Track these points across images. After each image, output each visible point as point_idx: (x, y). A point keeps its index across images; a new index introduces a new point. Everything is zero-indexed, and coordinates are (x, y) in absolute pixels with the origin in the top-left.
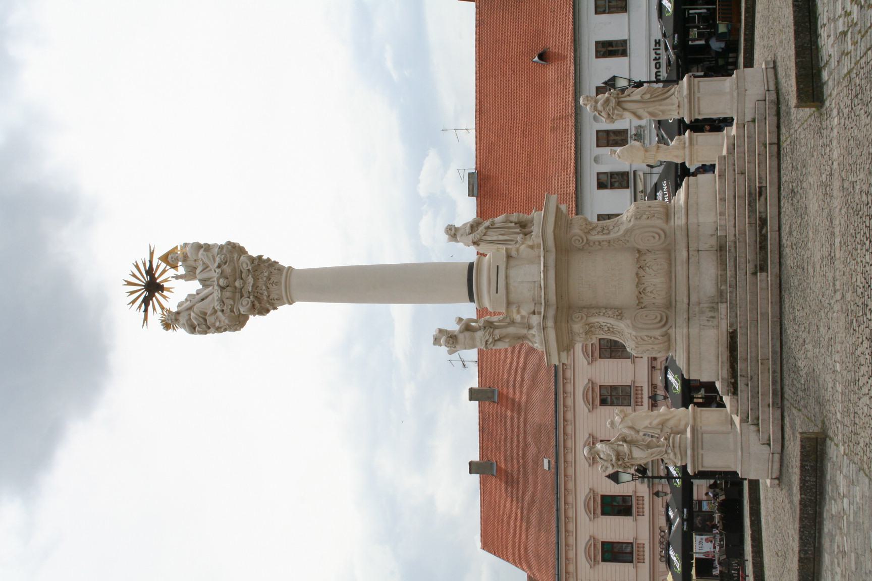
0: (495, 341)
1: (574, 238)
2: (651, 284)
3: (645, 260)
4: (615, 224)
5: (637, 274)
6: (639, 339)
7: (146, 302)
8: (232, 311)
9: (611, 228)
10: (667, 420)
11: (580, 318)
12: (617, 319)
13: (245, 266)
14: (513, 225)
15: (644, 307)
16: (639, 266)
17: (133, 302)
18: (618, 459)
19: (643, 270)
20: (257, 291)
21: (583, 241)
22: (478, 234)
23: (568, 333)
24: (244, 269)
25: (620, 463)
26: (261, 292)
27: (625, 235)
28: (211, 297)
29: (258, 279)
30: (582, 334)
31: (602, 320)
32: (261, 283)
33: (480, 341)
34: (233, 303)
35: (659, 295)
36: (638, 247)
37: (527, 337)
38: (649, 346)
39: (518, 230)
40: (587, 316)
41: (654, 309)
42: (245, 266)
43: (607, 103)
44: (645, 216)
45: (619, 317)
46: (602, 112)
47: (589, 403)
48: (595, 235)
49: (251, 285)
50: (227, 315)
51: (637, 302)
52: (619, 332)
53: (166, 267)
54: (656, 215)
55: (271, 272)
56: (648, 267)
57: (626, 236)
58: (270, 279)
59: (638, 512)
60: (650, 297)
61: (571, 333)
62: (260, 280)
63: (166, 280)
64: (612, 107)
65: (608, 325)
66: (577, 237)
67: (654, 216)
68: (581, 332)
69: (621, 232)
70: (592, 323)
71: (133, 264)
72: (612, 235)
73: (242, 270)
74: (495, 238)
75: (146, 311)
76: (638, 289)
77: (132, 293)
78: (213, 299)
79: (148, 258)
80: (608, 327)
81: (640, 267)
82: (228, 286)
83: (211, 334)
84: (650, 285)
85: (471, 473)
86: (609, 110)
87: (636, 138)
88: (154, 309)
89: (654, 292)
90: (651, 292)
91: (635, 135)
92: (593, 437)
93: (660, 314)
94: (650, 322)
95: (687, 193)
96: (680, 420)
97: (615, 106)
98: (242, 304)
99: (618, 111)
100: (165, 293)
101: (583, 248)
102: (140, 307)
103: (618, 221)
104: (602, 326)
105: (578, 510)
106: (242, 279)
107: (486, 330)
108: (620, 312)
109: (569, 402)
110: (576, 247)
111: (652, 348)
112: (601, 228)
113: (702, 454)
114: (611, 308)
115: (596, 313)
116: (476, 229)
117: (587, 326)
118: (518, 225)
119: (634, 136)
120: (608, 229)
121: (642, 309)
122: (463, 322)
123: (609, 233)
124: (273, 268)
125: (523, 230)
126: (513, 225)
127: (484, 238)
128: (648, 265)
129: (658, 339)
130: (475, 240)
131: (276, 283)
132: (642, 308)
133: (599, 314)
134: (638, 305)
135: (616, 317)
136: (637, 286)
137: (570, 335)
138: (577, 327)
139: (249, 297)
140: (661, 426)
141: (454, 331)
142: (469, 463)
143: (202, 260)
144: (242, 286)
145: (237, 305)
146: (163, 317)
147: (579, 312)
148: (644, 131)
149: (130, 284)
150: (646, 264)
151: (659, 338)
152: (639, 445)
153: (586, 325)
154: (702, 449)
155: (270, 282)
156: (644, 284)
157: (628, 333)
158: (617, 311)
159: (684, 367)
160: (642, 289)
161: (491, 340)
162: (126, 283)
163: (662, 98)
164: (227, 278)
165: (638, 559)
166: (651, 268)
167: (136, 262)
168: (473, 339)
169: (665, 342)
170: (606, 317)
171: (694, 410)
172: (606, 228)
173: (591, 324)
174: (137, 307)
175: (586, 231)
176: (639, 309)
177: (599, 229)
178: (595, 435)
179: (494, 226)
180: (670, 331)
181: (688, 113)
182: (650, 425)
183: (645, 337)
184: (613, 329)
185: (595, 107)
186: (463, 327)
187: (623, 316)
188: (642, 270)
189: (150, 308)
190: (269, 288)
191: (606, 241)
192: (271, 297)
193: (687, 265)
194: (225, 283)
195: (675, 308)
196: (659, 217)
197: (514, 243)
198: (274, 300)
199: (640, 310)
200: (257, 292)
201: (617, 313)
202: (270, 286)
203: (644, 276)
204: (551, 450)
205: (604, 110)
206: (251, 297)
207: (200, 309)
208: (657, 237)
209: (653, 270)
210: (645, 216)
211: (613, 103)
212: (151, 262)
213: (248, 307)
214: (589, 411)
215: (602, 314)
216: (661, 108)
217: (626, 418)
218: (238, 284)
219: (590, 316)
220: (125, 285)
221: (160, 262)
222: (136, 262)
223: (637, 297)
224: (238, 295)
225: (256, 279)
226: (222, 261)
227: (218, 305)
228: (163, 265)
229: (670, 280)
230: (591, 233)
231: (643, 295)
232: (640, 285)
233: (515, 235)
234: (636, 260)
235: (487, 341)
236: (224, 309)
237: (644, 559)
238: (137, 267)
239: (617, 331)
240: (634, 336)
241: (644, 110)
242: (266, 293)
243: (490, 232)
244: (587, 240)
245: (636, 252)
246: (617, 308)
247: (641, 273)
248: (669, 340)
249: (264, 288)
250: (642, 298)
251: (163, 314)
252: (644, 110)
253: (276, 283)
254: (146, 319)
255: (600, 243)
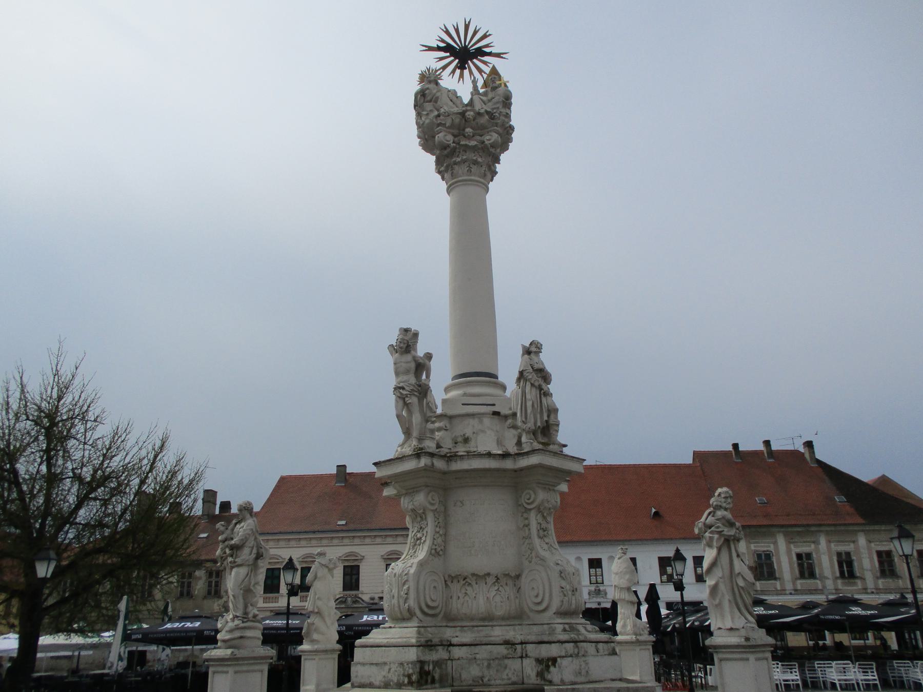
0: (404, 399)
1: (531, 492)
2: (476, 594)
3: (506, 584)
4: (551, 545)
5: (489, 574)
6: (405, 578)
7: (448, 48)
8: (439, 125)
9: (547, 540)
10: (323, 618)
11: (432, 502)
12: (432, 549)
13: (488, 137)
14: (545, 418)
15: (446, 585)
16: (499, 576)
17: (447, 32)
18: (232, 548)
19: (495, 582)
20: (461, 151)
21: (528, 504)
22: (533, 376)
23: (413, 488)
25: (228, 551)
26: (460, 155)
27: (538, 557)
28: (454, 106)
29: (474, 153)
30: (413, 504)
31: (430, 528)
32: (472, 156)
33: (403, 380)
35: (463, 604)
36: (524, 576)
37: (409, 438)
38: (397, 591)
39: (539, 424)
40: (434, 511)
41: (445, 599)
42: (488, 137)
43: (727, 524)
44: (564, 584)
45: (433, 551)
46: (713, 516)
47: (389, 555)
48: (537, 520)
49: (467, 143)
50: (434, 120)
51: (453, 575)
52: (415, 552)
53: (485, 73)
54: (566, 598)
55: (481, 166)
56: (499, 588)
57: (539, 559)
58: (475, 165)
59: (303, 597)
60: (460, 591)
61: (413, 492)
62: (474, 154)
63: (471, 73)
64: (723, 531)
65: (423, 538)
66: (533, 496)
67: (565, 596)
68: (415, 503)
69: (542, 553)
70: (426, 518)
71: (487, 32)
72: (537, 541)
74: (528, 396)
75: (439, 49)
76: (470, 576)
77: (457, 31)
78: (453, 108)
79: (494, 50)
80: (421, 538)
81: (498, 579)
82: (466, 121)
83: (416, 133)
84: (476, 592)
85: (338, 466)
86: (718, 527)
87: (597, 591)
88: (441, 59)
89: (467, 598)
90: (466, 593)
91: (599, 590)
92: (362, 559)
93: (439, 605)
94: (427, 592)
96: (323, 634)
97: (724, 535)
98: (446, 135)
99: (718, 539)
100: (458, 71)
101: (520, 505)
102: (443, 41)
103: (555, 549)
104: (423, 531)
105: (304, 549)
107: (416, 386)
108: (441, 553)
109: (389, 540)
110: (521, 496)
111: (393, 596)
112: (546, 528)
113: (227, 672)
114: (445, 542)
115: (439, 523)
116: (539, 375)
117: (421, 511)
118: (545, 424)
119: (598, 588)
120: (545, 536)
121: (444, 582)
122: (427, 361)
123: (540, 537)
124: (487, 170)
125: (539, 431)
126: (545, 418)
127: (528, 384)
128: (501, 589)
129: (405, 603)
130: (525, 373)
131: (470, 171)
132: (445, 581)
133: (437, 526)
134: (450, 576)
135: (434, 547)
136: (473, 575)
137: (412, 491)
138: (420, 499)
140: (316, 610)
141: (415, 350)
142: (345, 465)
144: (466, 135)
146: (432, 70)
147: (439, 501)
148: (602, 597)
149: (467, 27)
150: (502, 586)
151: (406, 605)
152: (250, 576)
153: (424, 510)
154: (236, 672)
156: (476, 583)
157: (412, 564)
158: (441, 550)
159: (371, 640)
160: (470, 582)
161: (404, 392)
163: (739, 605)
164: (474, 120)
165: (266, 598)
166: (497, 593)
167: (490, 35)
168: (407, 372)
169: (401, 613)
170: (434, 535)
171: (333, 651)
172: (545, 533)
173: (425, 516)
174: (443, 38)
175: (542, 508)
176: (444, 579)
177: (544, 525)
178: (364, 561)
179: (542, 396)
180: (415, 619)
181: (732, 644)
182: (318, 598)
183: (407, 586)
184: (419, 545)
185: (721, 506)
186: (421, 361)
187: (435, 557)
188: (495, 580)
189: (442, 54)
190: (464, 163)
191: (530, 533)
192: (456, 167)
194: (469, 117)
195: (447, 626)
196: (564, 602)
197: (524, 420)
199: (443, 580)
201: (439, 549)
202: (467, 164)
203: (486, 584)
204: (352, 526)
205: (717, 520)
206: (454, 145)
207: (440, 97)
208: (539, 600)
209: (495, 595)
210: (564, 584)
211: (728, 531)
212: (490, 54)
213: (445, 142)
214: (382, 556)
215: (438, 529)
216: (726, 604)
217: (326, 570)
218: (468, 130)
219: (435, 515)
221: (491, 66)
222: (490, 35)
223: (460, 575)
224: (456, 132)
225: (474, 149)
227: (445, 110)
228: (487, 70)
229: (483, 619)
230: (539, 515)
231: (462, 582)
232: (475, 578)
233: (532, 420)
234: (507, 573)
235: (403, 388)
236: (441, 116)
237: (266, 603)
238: (485, 36)
239: (417, 549)
240: (409, 571)
241: (721, 578)
242: (459, 159)
243: (535, 392)
244: (530, 510)
245: (517, 574)
246: (444, 550)
247: (491, 580)
248: (403, 619)
249: (464, 157)
250: (458, 581)
251: (436, 71)
252: (721, 578)
253: (470, 171)
254: (430, 49)
255: (527, 525)
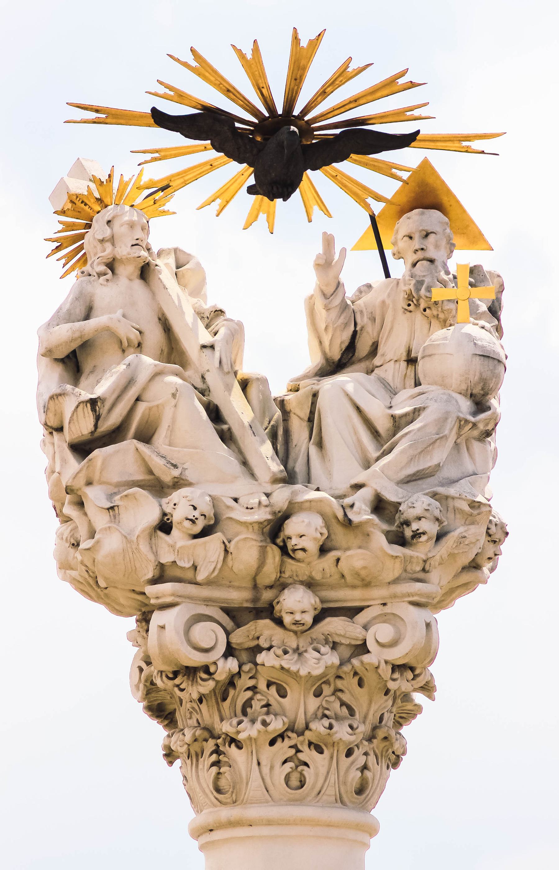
24: (366, 627)
34: (201, 577)
55: (349, 753)
73: (362, 618)
95: (376, 88)
106: (317, 620)
124: (372, 759)
139: (230, 652)
143: (417, 412)
144: (287, 619)
145: (191, 598)
155: (305, 748)
162: (304, 43)
193: (268, 786)
198: (216, 763)
200: (253, 689)
206: (232, 664)
220: (296, 39)
226: (407, 523)
